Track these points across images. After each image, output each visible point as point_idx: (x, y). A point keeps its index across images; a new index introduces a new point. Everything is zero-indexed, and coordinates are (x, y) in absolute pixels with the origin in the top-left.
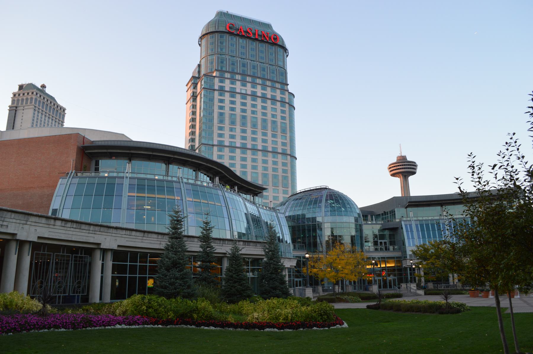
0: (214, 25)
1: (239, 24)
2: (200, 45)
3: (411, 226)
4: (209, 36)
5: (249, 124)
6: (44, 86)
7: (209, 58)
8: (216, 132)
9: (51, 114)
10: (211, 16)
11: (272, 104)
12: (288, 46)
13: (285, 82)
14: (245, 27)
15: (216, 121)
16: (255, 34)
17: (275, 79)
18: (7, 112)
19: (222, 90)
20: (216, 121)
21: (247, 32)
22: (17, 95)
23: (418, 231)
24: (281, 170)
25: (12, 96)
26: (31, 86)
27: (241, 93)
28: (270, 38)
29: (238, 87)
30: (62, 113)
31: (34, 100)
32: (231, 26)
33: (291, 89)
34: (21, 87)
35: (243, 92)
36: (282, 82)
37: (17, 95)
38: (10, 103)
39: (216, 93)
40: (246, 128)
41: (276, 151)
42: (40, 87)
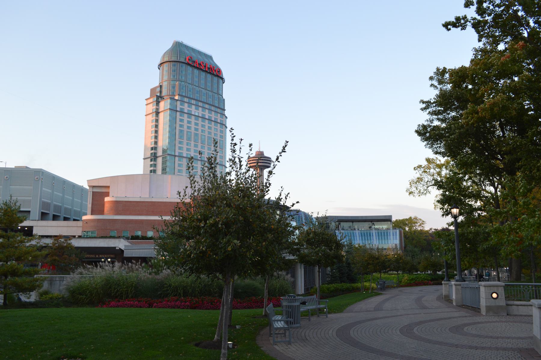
0: (176, 55)
1: (195, 57)
2: (159, 68)
4: (172, 63)
7: (172, 83)
8: (178, 145)
10: (169, 46)
11: (188, 117)
14: (200, 59)
16: (205, 66)
17: (192, 97)
21: (200, 64)
28: (215, 71)
32: (191, 58)
33: (226, 113)
35: (197, 114)
36: (219, 106)
41: (181, 155)
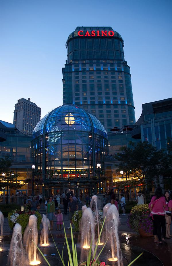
3: (150, 128)
5: (96, 89)
6: (29, 99)
9: (33, 111)
12: (123, 39)
13: (120, 59)
15: (74, 90)
18: (13, 114)
19: (77, 71)
20: (74, 90)
22: (17, 105)
23: (157, 133)
24: (121, 116)
25: (15, 106)
26: (23, 99)
27: (89, 71)
29: (87, 67)
30: (39, 111)
31: (25, 106)
34: (19, 101)
37: (17, 105)
38: (14, 110)
39: (73, 74)
40: (94, 92)
42: (27, 100)
